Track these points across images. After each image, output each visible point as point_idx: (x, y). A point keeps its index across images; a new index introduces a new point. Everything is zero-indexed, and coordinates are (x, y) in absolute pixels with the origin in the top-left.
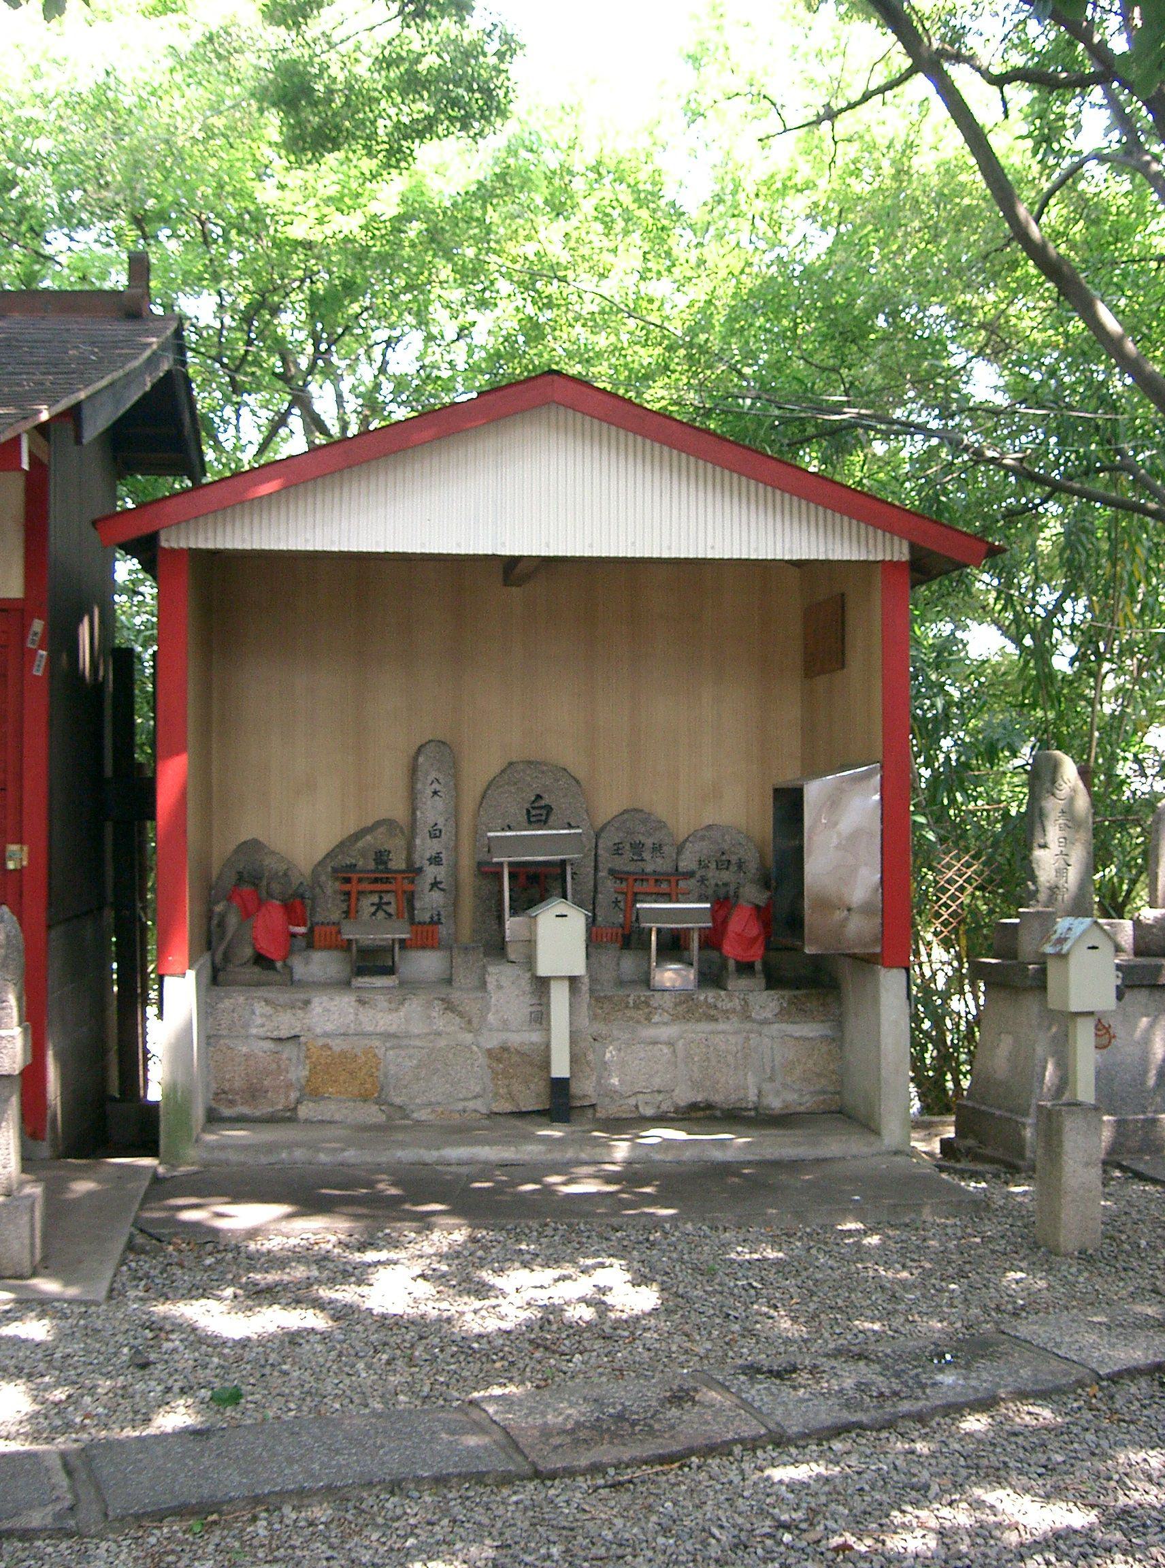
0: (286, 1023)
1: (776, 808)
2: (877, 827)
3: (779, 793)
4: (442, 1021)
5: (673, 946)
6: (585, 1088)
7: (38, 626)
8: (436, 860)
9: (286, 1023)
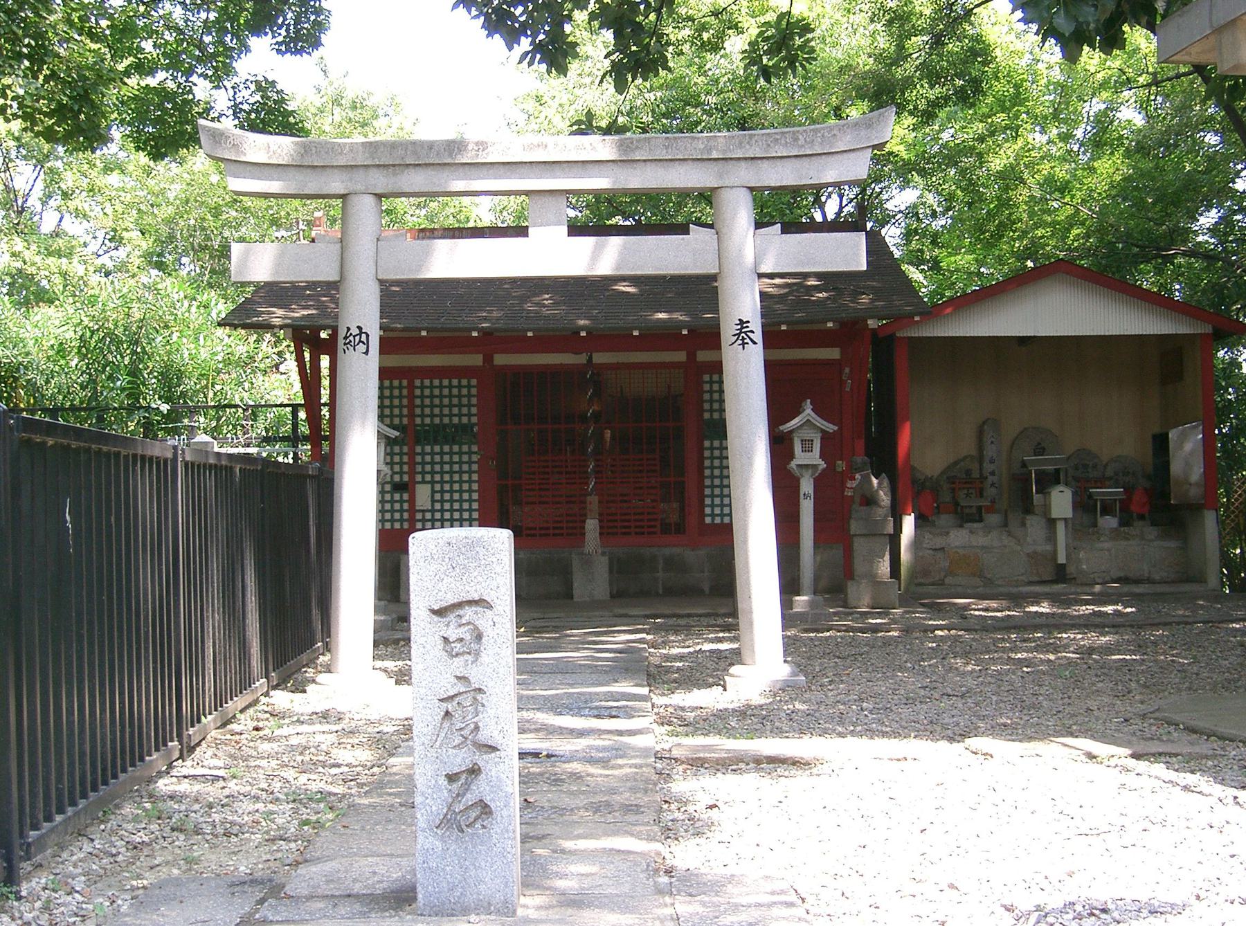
0: (939, 542)
1: (748, 578)
2: (1201, 449)
3: (1155, 437)
4: (1006, 540)
5: (1106, 510)
6: (1071, 569)
7: (847, 370)
8: (993, 473)
9: (939, 542)
